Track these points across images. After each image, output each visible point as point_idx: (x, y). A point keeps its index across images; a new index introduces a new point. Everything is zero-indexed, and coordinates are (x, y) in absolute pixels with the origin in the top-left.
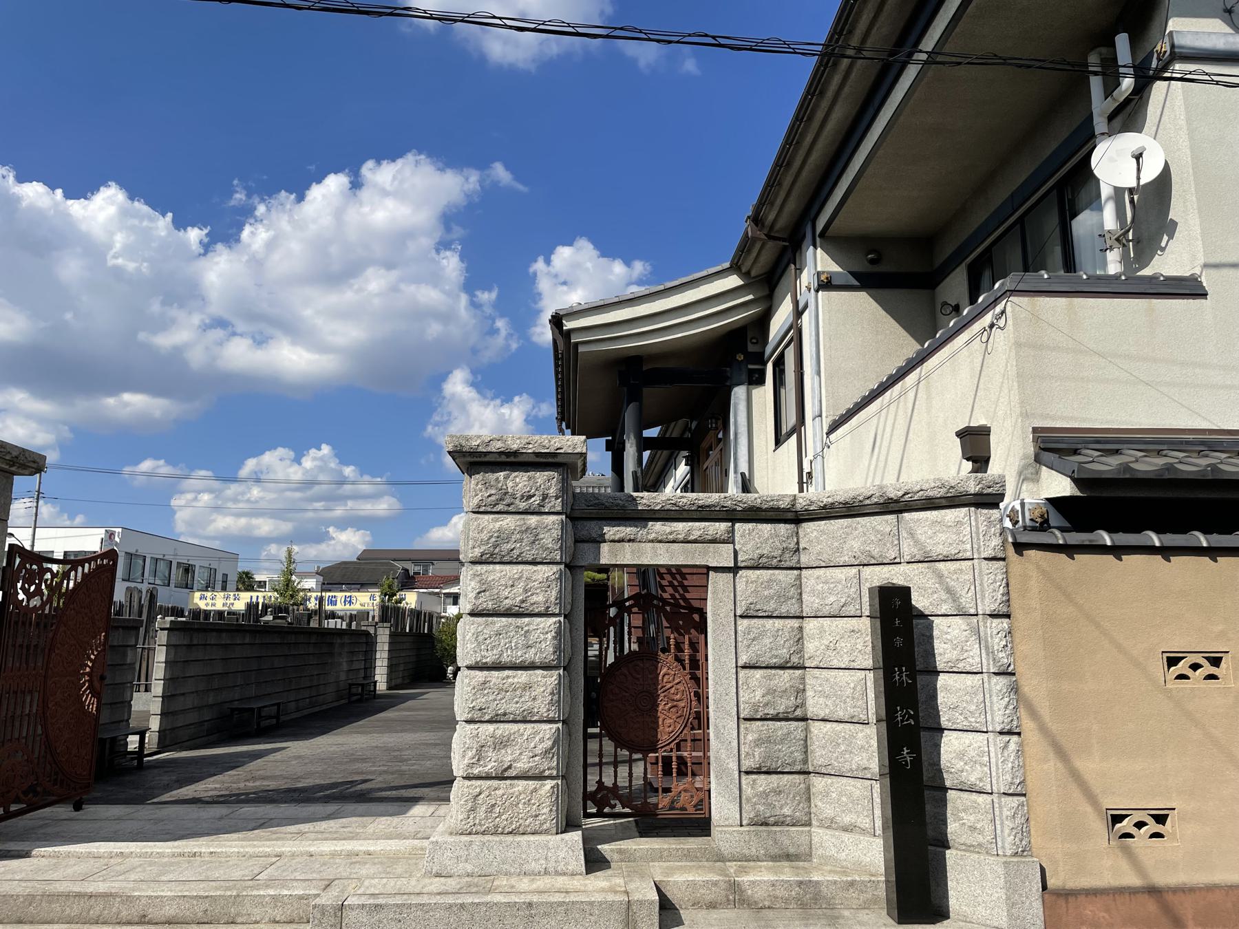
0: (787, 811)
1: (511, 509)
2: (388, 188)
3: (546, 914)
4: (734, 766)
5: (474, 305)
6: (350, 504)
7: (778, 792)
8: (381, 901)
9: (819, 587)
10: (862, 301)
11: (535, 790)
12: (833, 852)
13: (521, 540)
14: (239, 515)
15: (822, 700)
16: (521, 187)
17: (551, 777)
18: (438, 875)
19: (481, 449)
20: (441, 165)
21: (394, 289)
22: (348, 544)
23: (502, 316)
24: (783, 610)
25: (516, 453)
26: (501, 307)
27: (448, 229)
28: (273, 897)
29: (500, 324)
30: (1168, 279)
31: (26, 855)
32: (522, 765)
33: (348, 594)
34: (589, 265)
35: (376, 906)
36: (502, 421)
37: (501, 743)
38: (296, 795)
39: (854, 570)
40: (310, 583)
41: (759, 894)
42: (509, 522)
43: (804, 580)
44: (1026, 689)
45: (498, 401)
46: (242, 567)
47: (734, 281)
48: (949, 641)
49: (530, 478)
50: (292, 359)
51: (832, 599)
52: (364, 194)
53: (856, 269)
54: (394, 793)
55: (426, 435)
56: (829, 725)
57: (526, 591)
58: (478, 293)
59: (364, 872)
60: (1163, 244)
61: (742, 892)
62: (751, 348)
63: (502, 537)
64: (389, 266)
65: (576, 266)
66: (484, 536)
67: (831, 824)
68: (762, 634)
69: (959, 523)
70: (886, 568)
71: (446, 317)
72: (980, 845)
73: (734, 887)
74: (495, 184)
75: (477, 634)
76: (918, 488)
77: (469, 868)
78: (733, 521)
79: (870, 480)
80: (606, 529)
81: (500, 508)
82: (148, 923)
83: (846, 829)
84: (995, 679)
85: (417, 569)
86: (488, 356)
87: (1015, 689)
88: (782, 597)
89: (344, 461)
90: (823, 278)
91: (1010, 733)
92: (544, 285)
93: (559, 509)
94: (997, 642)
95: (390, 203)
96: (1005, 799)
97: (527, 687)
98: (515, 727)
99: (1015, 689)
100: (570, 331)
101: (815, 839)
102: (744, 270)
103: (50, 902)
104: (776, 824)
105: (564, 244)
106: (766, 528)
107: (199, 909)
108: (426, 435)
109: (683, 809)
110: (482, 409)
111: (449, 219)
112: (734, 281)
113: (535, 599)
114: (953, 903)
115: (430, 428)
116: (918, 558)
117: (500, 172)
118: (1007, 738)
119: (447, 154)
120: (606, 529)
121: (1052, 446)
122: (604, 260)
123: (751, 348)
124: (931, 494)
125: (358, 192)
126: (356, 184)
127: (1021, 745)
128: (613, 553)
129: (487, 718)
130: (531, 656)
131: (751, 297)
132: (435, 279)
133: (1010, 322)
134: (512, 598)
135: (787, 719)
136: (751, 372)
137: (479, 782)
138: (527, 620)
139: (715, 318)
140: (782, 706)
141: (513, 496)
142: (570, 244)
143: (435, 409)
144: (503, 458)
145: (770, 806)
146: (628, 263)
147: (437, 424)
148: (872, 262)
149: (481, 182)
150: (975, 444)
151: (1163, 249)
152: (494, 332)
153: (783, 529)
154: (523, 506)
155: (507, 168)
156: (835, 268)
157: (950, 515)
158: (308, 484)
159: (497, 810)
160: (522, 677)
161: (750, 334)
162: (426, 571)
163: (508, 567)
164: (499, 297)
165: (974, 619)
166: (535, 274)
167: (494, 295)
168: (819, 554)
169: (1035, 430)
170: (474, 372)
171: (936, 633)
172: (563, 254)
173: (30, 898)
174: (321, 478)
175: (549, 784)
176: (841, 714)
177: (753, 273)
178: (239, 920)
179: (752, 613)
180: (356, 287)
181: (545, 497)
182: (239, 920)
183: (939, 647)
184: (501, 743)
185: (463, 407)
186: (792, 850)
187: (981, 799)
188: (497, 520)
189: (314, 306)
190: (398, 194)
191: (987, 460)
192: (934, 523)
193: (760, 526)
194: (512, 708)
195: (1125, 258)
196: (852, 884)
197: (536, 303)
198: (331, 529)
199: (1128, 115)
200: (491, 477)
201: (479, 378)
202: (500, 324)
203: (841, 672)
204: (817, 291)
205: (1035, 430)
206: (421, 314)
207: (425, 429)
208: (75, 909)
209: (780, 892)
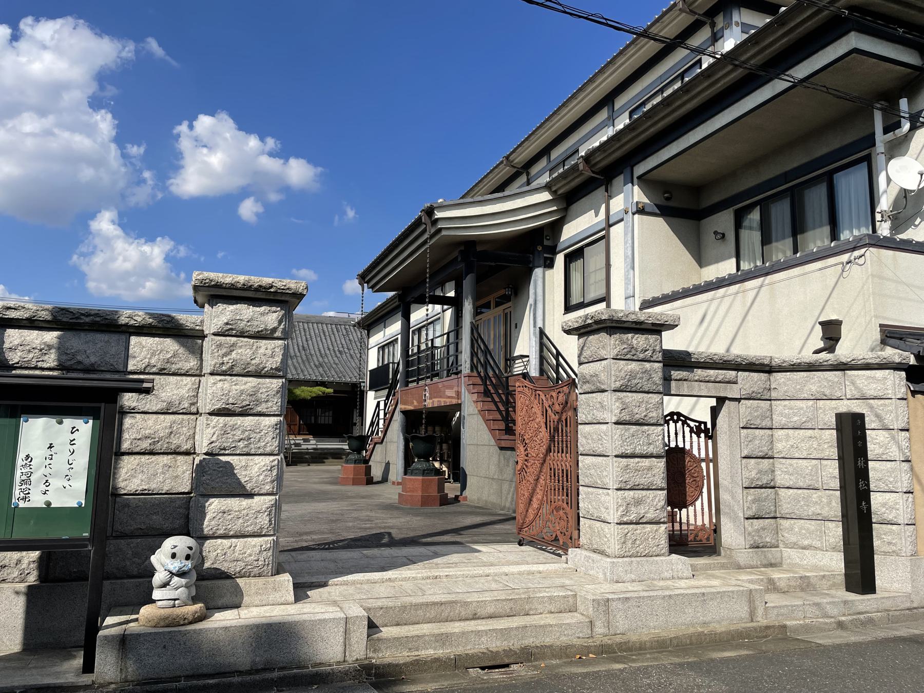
0: (768, 540)
1: (635, 358)
2: (48, 43)
3: (712, 599)
4: (741, 515)
5: (124, 156)
7: (763, 529)
8: (628, 595)
9: (786, 411)
10: (659, 224)
11: (657, 530)
12: (798, 560)
13: (642, 378)
15: (786, 477)
16: (174, 63)
17: (664, 523)
18: (617, 582)
19: (624, 319)
20: (98, 31)
21: (48, 133)
23: (149, 168)
24: (764, 424)
25: (642, 323)
26: (149, 160)
27: (102, 87)
28: (549, 597)
29: (147, 174)
30: (917, 242)
31: (324, 585)
32: (650, 516)
34: (228, 135)
35: (626, 598)
36: (145, 258)
37: (638, 502)
38: (359, 543)
39: (811, 403)
41: (782, 584)
42: (634, 366)
43: (774, 407)
44: (916, 469)
45: (143, 240)
47: (546, 196)
48: (876, 441)
49: (646, 339)
51: (796, 419)
52: (22, 45)
53: (657, 203)
54: (429, 540)
55: (71, 263)
56: (791, 491)
57: (647, 409)
58: (129, 146)
60: (917, 223)
61: (774, 584)
62: (546, 243)
63: (632, 375)
64: (42, 112)
65: (214, 133)
66: (623, 374)
67: (794, 546)
68: (754, 438)
69: (885, 378)
70: (834, 402)
71: (97, 162)
72: (894, 552)
73: (771, 581)
74: (150, 55)
75: (621, 435)
76: (861, 357)
77: (633, 576)
78: (738, 370)
79: (695, 342)
80: (672, 372)
81: (628, 356)
82: (478, 619)
83: (804, 548)
84: (904, 464)
86: (132, 201)
87: (912, 469)
88: (763, 417)
90: (640, 206)
91: (909, 492)
92: (185, 144)
93: (660, 359)
94: (905, 444)
95: (48, 57)
96: (907, 527)
97: (650, 468)
98: (644, 493)
99: (912, 469)
100: (437, 220)
101: (785, 555)
102: (554, 189)
103: (416, 610)
104: (763, 547)
105: (206, 114)
106: (755, 375)
107: (507, 607)
108: (71, 263)
109: (701, 540)
110: (126, 246)
111: (103, 77)
112: (546, 196)
113: (651, 415)
114: (878, 582)
115: (75, 257)
116: (856, 397)
117: (153, 45)
118: (907, 495)
119: (102, 24)
120: (672, 372)
121: (891, 335)
122: (242, 133)
123: (546, 243)
124: (870, 361)
125: (15, 44)
126: (15, 37)
127: (914, 498)
128: (678, 388)
129: (628, 487)
130: (651, 449)
131: (555, 208)
132: (89, 130)
133: (868, 262)
134: (640, 413)
135: (766, 488)
136: (546, 259)
137: (626, 526)
138: (646, 427)
139: (531, 221)
140: (764, 481)
141: (636, 350)
142: (213, 115)
143: (82, 242)
144: (634, 326)
145: (760, 537)
146: (262, 139)
147: (83, 255)
148: (667, 199)
149: (137, 52)
150: (831, 332)
151: (916, 226)
152: (141, 182)
153: (763, 376)
154: (641, 356)
155: (160, 45)
156: (646, 200)
157: (879, 374)
159: (638, 542)
160: (646, 462)
161: (545, 233)
163: (634, 394)
164: (146, 151)
165: (893, 432)
166: (179, 136)
167: (142, 150)
168: (786, 392)
169: (881, 326)
170: (121, 215)
171: (868, 439)
172: (204, 122)
173: (404, 608)
175: (663, 527)
176: (801, 484)
177: (560, 192)
178: (531, 612)
179: (748, 426)
180: (10, 125)
181: (654, 351)
182: (531, 612)
183: (870, 446)
184: (638, 502)
185: (108, 241)
186: (773, 561)
187: (894, 527)
188: (627, 365)
190: (58, 50)
191: (837, 340)
192: (868, 377)
193: (752, 374)
194: (642, 481)
195: (892, 229)
196: (824, 576)
197: (178, 160)
199: (897, 148)
200: (625, 336)
201: (125, 220)
202: (147, 174)
203: (801, 461)
204: (634, 214)
205: (881, 326)
206: (73, 158)
207: (71, 258)
208: (432, 613)
209: (793, 583)
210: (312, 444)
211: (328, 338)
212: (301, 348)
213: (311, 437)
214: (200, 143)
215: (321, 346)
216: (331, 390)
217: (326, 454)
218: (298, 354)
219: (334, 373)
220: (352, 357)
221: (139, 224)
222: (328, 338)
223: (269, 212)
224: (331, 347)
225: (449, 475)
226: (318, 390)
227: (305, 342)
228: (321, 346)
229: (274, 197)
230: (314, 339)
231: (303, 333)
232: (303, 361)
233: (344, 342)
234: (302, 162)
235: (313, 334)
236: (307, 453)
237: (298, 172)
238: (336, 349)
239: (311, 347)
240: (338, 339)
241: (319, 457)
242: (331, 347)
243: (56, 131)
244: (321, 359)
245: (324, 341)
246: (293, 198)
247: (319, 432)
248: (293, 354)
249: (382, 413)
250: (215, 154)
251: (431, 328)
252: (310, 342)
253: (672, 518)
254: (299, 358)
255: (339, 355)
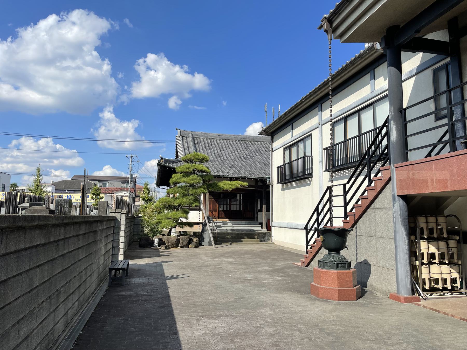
6: (61, 160)
14: (8, 163)
22: (61, 175)
33: (69, 195)
40: (49, 189)
46: (12, 182)
50: (31, 96)
59: (140, 289)
65: (155, 62)
85: (101, 184)
89: (56, 143)
111: (102, 38)
132: (99, 67)
142: (156, 54)
155: (131, 21)
158: (39, 151)
162: (105, 186)
174: (46, 149)
189: (43, 74)
198: (53, 171)
210: (229, 226)
211: (234, 148)
212: (217, 155)
213: (227, 220)
214: (149, 68)
215: (231, 154)
216: (246, 184)
217: (242, 234)
218: (216, 159)
219: (245, 172)
220: (254, 162)
221: (123, 113)
222: (234, 148)
223: (185, 103)
224: (237, 155)
225: (461, 282)
226: (236, 184)
227: (219, 152)
228: (231, 154)
229: (187, 96)
230: (225, 150)
231: (217, 146)
232: (220, 164)
233: (246, 152)
234: (202, 75)
235: (224, 146)
236: (228, 234)
237: (199, 81)
238: (242, 156)
239: (224, 155)
240: (242, 149)
241: (237, 237)
242: (237, 155)
243: (84, 67)
244: (232, 163)
245: (232, 151)
246: (197, 96)
247: (232, 216)
248: (212, 160)
249: (338, 201)
250: (158, 75)
251: (301, 146)
252: (223, 152)
253: (427, 264)
254: (217, 162)
255: (244, 160)
